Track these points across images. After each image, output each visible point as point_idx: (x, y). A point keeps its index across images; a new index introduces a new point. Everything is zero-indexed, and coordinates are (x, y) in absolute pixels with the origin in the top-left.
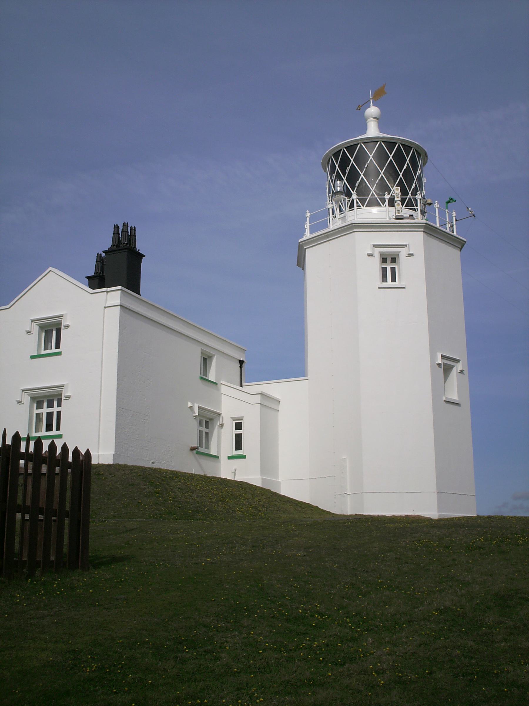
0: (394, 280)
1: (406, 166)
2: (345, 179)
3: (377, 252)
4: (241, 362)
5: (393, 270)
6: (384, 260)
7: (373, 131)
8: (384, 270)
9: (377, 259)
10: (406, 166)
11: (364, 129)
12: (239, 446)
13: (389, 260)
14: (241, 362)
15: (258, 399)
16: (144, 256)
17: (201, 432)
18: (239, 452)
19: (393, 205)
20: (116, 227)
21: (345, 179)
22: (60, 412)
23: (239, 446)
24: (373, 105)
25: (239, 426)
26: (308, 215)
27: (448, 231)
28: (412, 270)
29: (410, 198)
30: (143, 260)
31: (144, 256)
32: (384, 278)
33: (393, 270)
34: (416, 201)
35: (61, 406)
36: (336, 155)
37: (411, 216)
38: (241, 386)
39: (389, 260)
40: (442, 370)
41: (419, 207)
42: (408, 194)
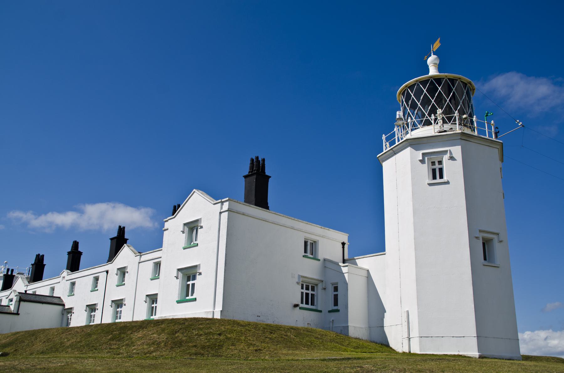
0: (441, 177)
6: (433, 163)
7: (433, 71)
8: (434, 171)
11: (427, 71)
12: (336, 303)
13: (437, 163)
16: (270, 177)
17: (302, 293)
18: (336, 308)
20: (252, 160)
22: (337, 295)
23: (336, 303)
24: (434, 54)
25: (336, 289)
26: (384, 137)
27: (487, 137)
28: (454, 170)
30: (270, 180)
31: (270, 177)
32: (434, 177)
35: (38, 256)
36: (411, 87)
39: (437, 163)
41: (457, 122)
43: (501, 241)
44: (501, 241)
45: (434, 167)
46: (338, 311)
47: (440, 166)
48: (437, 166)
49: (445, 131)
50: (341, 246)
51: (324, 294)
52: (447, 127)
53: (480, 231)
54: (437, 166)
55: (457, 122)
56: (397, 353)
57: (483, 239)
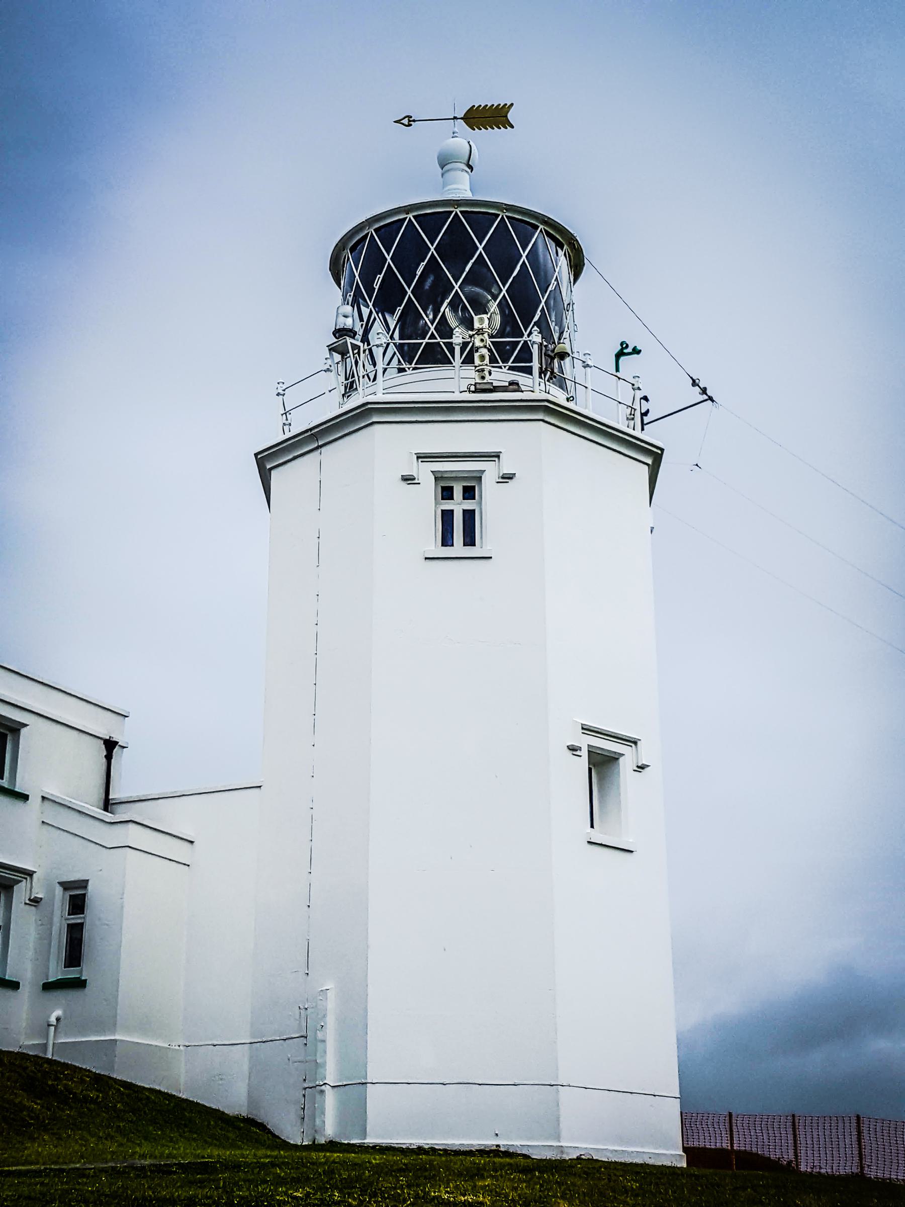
0: (470, 540)
1: (539, 313)
2: (371, 305)
3: (425, 473)
4: (110, 745)
5: (469, 516)
6: (447, 493)
8: (447, 516)
9: (428, 487)
10: (539, 313)
14: (110, 745)
15: (523, 388)
19: (469, 360)
21: (371, 305)
22: (80, 926)
25: (78, 904)
29: (526, 342)
32: (447, 540)
33: (469, 516)
34: (451, 347)
37: (514, 386)
38: (106, 809)
40: (583, 762)
42: (523, 335)
43: (642, 767)
44: (642, 767)
45: (447, 505)
46: (79, 984)
47: (469, 505)
48: (458, 506)
49: (495, 389)
50: (46, 826)
51: (489, 301)
52: (501, 375)
53: (586, 729)
54: (458, 506)
55: (535, 365)
56: (285, 1145)
57: (438, 477)
